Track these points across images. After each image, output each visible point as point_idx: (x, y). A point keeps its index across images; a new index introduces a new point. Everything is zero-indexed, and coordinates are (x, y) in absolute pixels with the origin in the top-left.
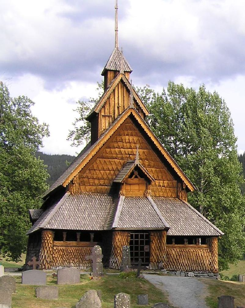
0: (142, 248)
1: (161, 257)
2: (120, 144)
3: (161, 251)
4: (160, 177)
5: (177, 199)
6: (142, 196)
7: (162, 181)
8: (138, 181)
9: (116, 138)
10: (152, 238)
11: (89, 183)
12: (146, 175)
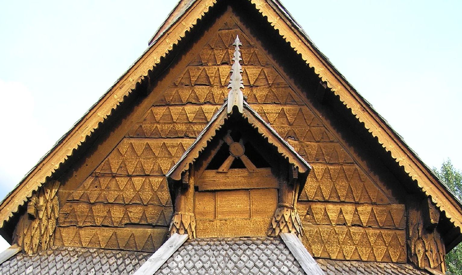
2: (202, 91)
4: (342, 193)
5: (407, 266)
6: (263, 235)
7: (349, 208)
8: (244, 180)
9: (188, 72)
11: (93, 217)
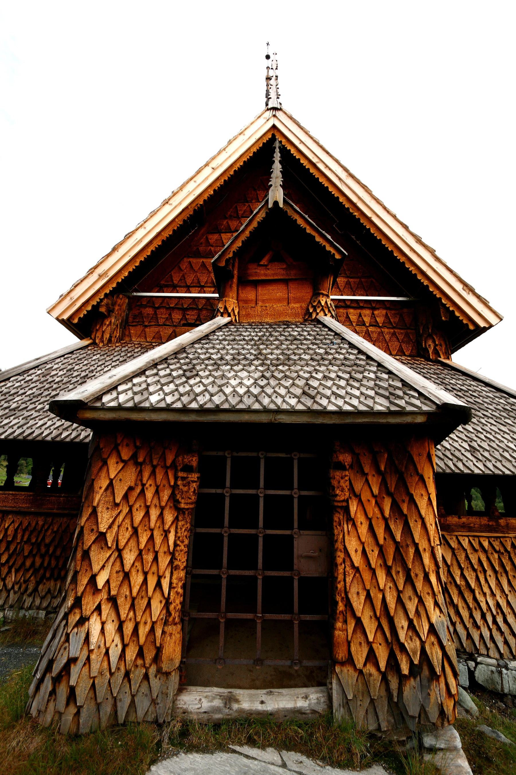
0: (281, 552)
1: (411, 626)
3: (409, 580)
8: (283, 272)
9: (236, 207)
10: (345, 484)
11: (157, 318)
12: (309, 234)
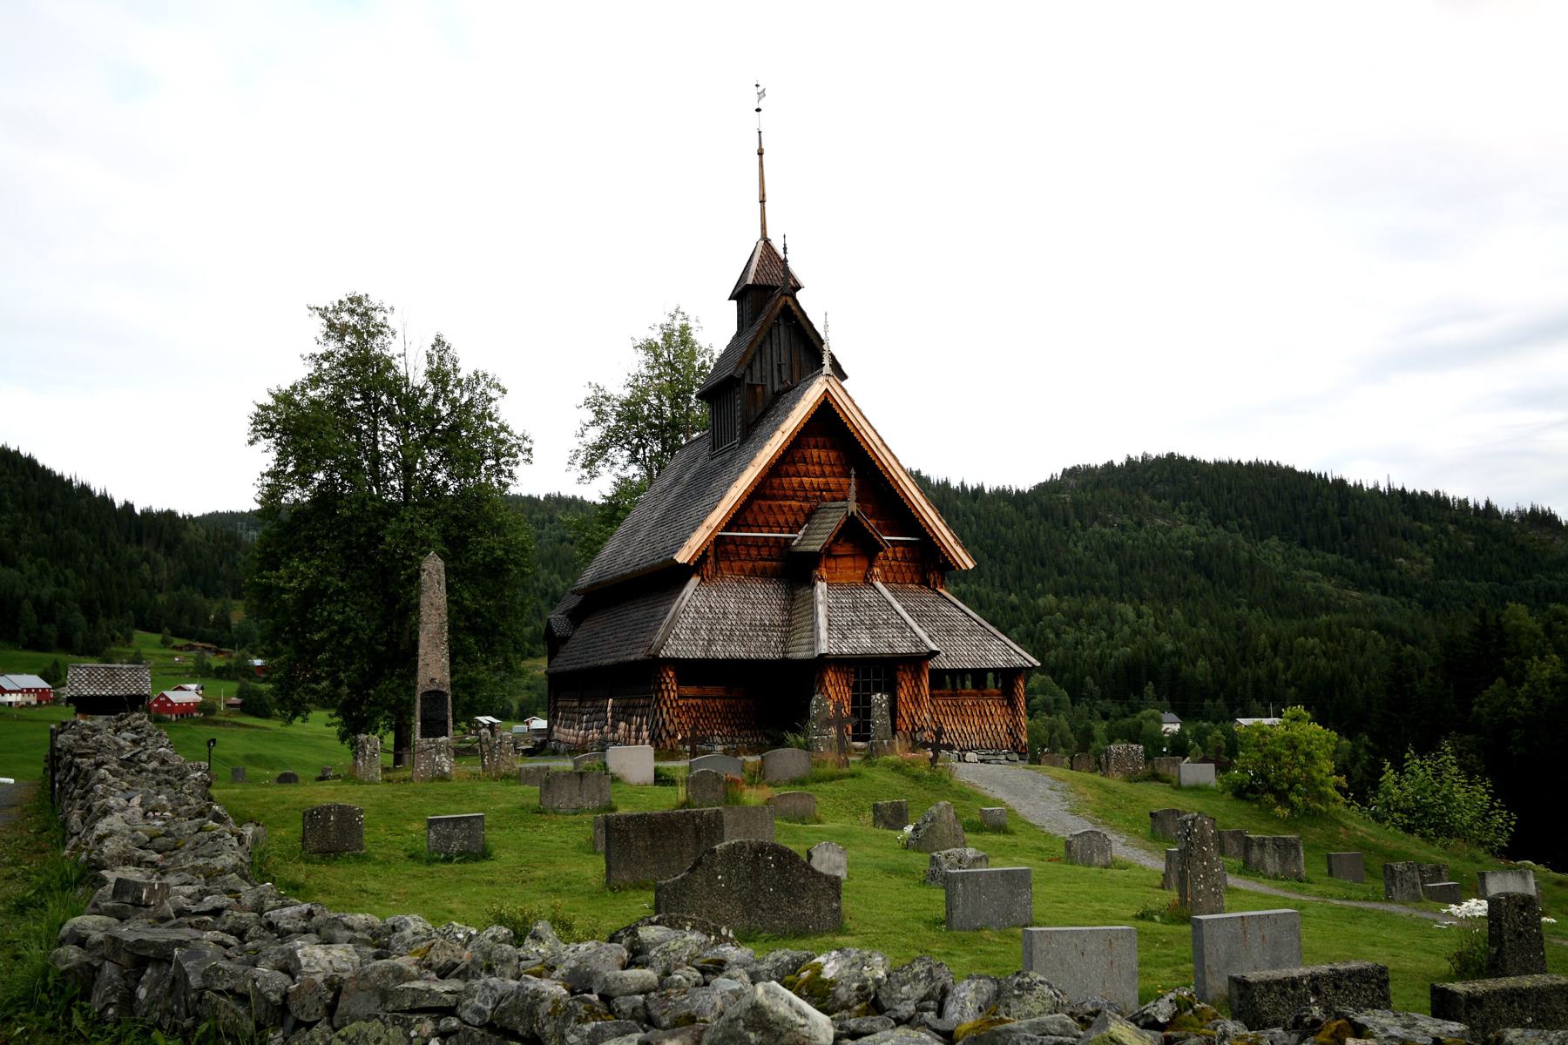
2: (802, 467)
